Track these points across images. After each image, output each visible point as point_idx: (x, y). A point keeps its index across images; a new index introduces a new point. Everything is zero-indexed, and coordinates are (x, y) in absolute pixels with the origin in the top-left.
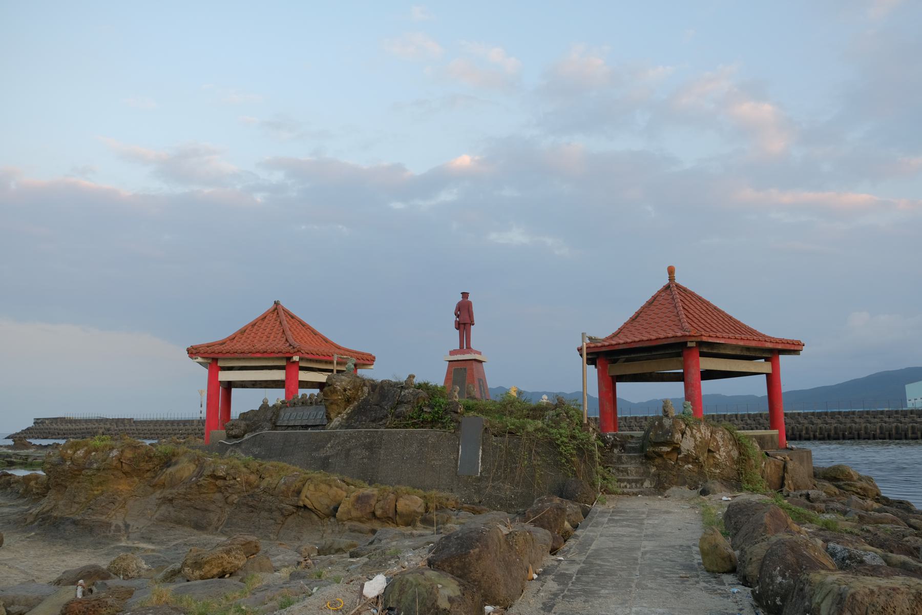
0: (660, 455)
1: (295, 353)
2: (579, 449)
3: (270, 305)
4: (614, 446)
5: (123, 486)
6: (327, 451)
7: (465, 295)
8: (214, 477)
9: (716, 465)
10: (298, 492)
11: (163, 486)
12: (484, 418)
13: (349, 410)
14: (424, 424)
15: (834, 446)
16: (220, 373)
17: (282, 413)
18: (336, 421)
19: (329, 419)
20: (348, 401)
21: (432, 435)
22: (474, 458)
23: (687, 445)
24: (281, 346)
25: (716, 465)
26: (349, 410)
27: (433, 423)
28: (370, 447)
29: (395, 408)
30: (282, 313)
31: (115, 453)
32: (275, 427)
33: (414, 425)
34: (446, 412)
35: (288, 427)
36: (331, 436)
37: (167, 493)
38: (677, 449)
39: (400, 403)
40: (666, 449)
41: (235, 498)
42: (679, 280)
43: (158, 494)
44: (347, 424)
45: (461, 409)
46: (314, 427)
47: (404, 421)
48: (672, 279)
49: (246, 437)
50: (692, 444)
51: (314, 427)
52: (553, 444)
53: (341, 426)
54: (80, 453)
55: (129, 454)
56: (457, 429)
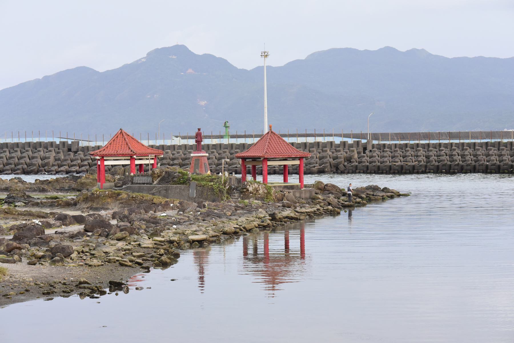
0: (244, 192)
1: (134, 155)
2: (219, 190)
3: (118, 130)
4: (234, 189)
5: (109, 200)
6: (154, 191)
7: (199, 130)
8: (133, 197)
9: (259, 194)
10: (152, 200)
11: (119, 200)
12: (196, 182)
13: (159, 179)
14: (181, 184)
15: (432, 176)
16: (105, 162)
17: (134, 178)
18: (155, 182)
19: (153, 182)
20: (159, 176)
21: (183, 186)
22: (193, 192)
23: (251, 189)
24: (130, 152)
25: (259, 194)
26: (159, 179)
27: (183, 183)
28: (166, 190)
29: (173, 179)
30: (124, 134)
31: (107, 193)
32: (132, 183)
33: (178, 184)
34: (187, 180)
35: (137, 183)
36: (154, 187)
37: (121, 201)
38: (248, 190)
39: (174, 178)
40: (245, 190)
41: (138, 202)
42: (273, 130)
43: (118, 202)
44: (159, 183)
45: (191, 179)
46: (147, 184)
47: (175, 183)
48: (271, 130)
49: (124, 187)
50: (116, 208)
51: (147, 184)
52: (213, 189)
53: (157, 184)
54: (98, 193)
55: (110, 193)
56: (189, 185)
